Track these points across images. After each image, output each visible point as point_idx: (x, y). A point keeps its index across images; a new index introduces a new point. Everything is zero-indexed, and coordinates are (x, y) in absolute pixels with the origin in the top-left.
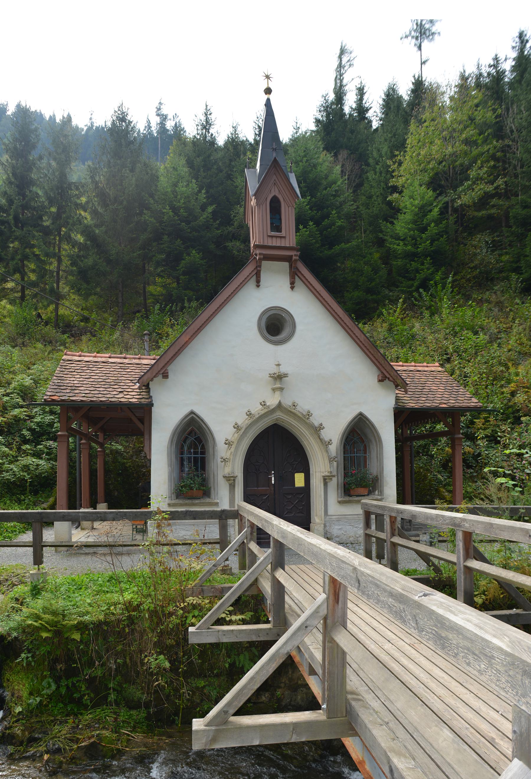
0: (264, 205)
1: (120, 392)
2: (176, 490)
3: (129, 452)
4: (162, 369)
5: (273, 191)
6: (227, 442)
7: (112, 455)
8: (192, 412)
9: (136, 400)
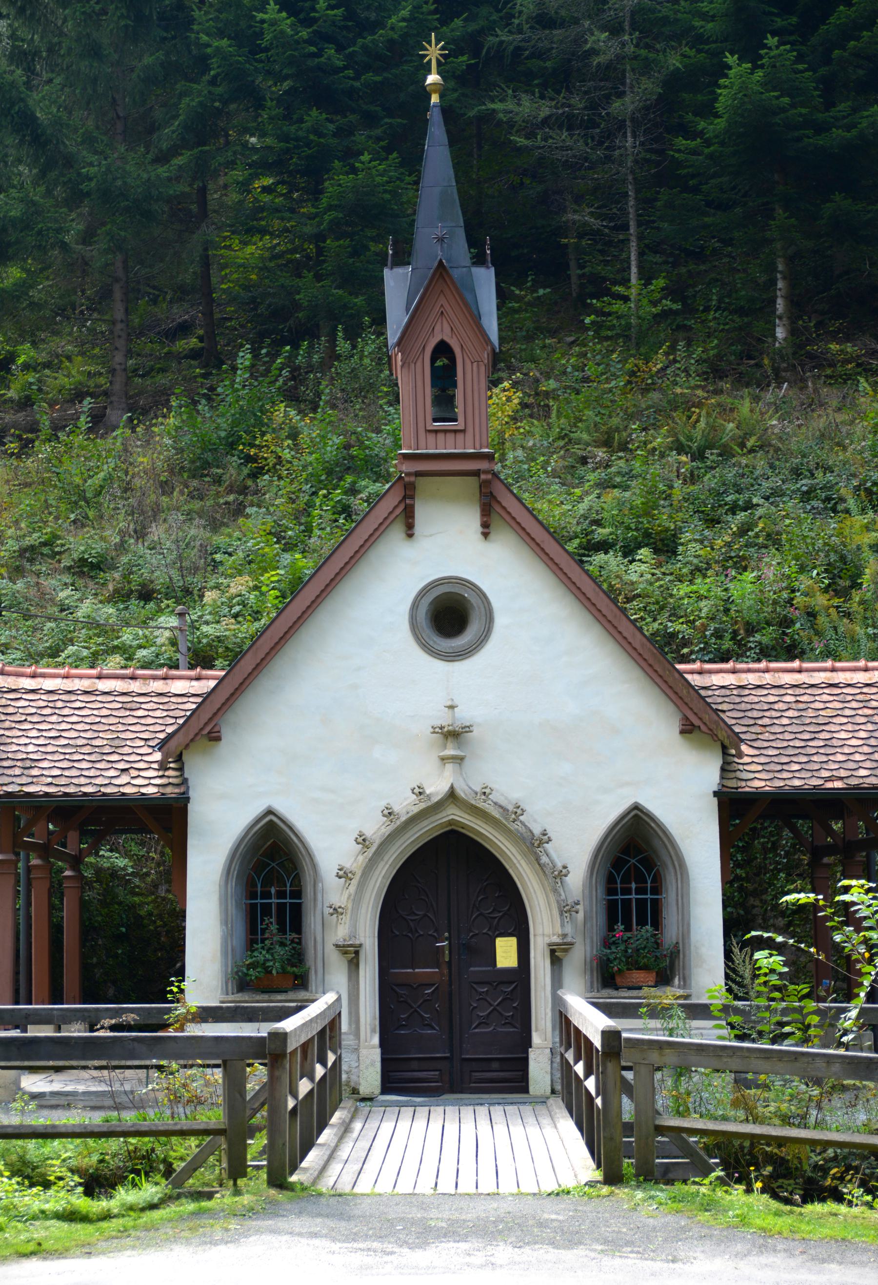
0: (419, 364)
1: (123, 770)
2: (237, 973)
3: (147, 874)
4: (206, 724)
5: (438, 327)
6: (341, 873)
7: (101, 883)
8: (270, 812)
9: (155, 790)
